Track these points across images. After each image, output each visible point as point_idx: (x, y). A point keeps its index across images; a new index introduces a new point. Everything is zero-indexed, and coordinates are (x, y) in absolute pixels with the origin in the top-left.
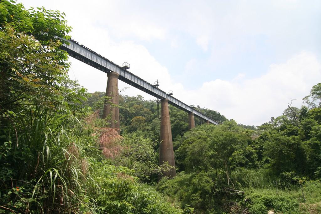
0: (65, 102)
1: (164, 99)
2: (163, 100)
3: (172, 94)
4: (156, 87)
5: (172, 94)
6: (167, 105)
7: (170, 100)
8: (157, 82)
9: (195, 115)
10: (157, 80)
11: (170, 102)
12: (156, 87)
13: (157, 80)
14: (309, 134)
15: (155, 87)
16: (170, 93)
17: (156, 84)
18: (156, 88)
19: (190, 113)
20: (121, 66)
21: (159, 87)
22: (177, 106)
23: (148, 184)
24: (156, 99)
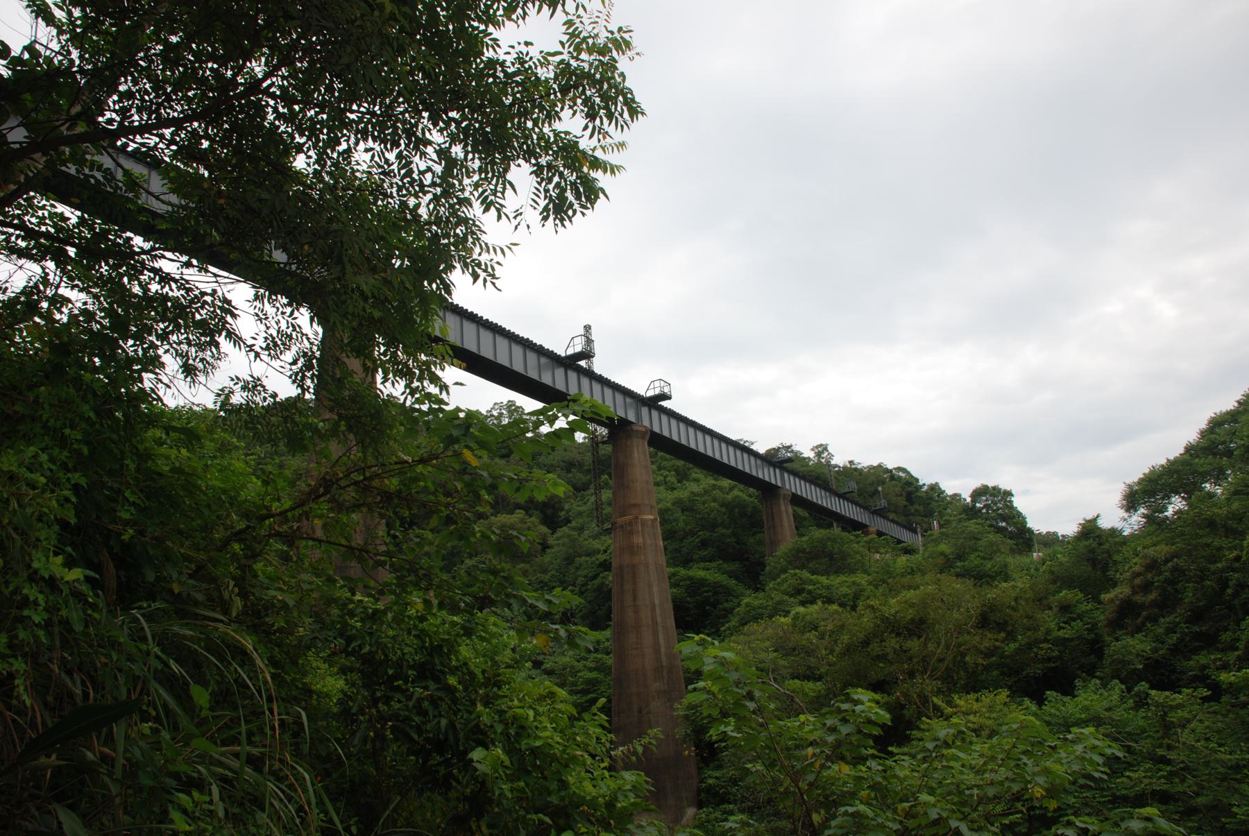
0: (166, 359)
1: (624, 422)
2: (619, 428)
3: (669, 398)
4: (583, 363)
5: (666, 397)
6: (640, 453)
7: (656, 429)
8: (589, 341)
9: (797, 500)
10: (587, 328)
11: (658, 442)
12: (583, 363)
13: (587, 328)
14: (189, 794)
15: (569, 363)
16: (657, 391)
17: (578, 349)
18: (580, 370)
19: (768, 491)
20: (561, 352)
21: (600, 366)
22: (689, 453)
23: (735, 631)
24: (504, 395)
